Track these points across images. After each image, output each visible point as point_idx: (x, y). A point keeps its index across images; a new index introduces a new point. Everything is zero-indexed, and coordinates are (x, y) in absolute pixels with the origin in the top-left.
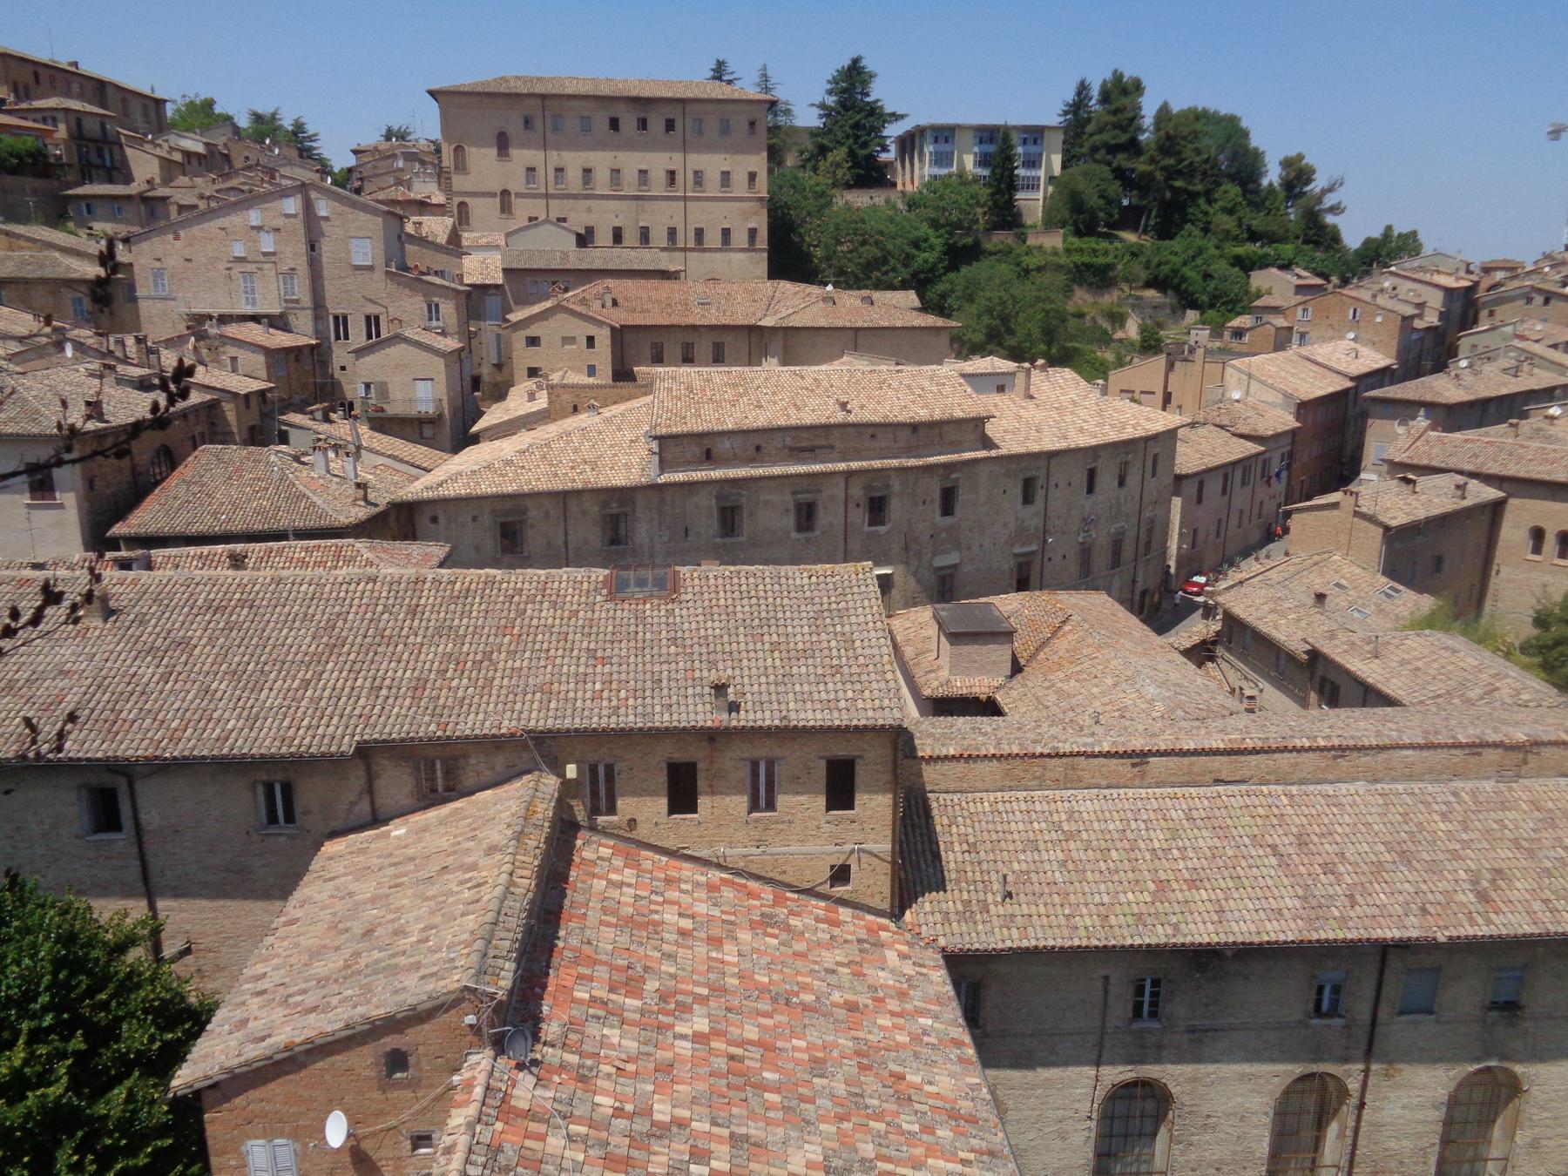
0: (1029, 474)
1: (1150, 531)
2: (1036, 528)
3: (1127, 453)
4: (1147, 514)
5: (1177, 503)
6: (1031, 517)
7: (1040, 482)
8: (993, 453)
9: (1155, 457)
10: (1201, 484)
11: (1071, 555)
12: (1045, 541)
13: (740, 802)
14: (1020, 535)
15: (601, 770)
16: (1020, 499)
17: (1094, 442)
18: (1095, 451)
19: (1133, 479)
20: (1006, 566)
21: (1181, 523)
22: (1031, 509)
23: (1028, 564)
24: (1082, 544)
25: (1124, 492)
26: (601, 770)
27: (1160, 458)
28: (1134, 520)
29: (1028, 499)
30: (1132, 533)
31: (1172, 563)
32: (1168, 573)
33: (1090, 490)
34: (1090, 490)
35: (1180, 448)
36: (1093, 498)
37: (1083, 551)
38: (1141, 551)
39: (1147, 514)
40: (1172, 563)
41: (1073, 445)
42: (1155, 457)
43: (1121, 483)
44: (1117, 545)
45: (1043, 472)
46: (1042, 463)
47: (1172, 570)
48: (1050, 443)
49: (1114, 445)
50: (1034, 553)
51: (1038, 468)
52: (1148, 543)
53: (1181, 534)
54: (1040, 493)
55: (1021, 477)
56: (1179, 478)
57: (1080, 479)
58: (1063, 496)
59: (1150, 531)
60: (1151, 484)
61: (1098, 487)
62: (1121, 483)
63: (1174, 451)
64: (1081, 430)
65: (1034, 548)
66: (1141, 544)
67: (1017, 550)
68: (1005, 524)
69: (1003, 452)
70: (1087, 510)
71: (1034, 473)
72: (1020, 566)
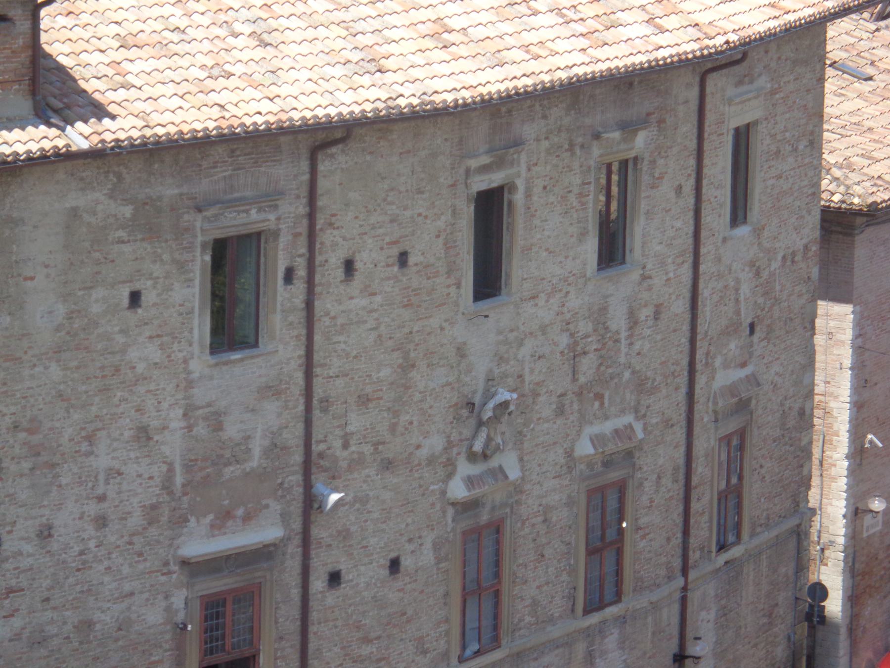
0: (233, 223)
1: (737, 445)
2: (275, 449)
3: (629, 128)
4: (721, 378)
5: (836, 325)
6: (250, 397)
7: (284, 253)
8: (80, 136)
9: (742, 139)
10: (480, 534)
11: (421, 559)
12: (311, 503)
13: (833, 468)
14: (206, 481)
15: (615, 167)
16: (201, 326)
17: (494, 82)
18: (500, 113)
19: (656, 231)
20: (154, 616)
21: (858, 406)
22: (246, 371)
23: (249, 597)
24: (469, 506)
25: (622, 287)
26: (615, 167)
27: (761, 145)
28: (668, 402)
29: (231, 327)
30: (665, 456)
31: (832, 576)
32: (815, 617)
33: (488, 282)
34: (488, 282)
35: (840, 101)
36: (499, 313)
37: (473, 535)
38: (704, 530)
39: (721, 378)
40: (832, 576)
41: (408, 98)
42: (742, 139)
43: (612, 249)
44: (606, 504)
45: (293, 208)
46: (289, 173)
47: (834, 605)
48: (313, 88)
49: (575, 93)
50: (264, 554)
51: (270, 199)
52: (731, 498)
53: (859, 454)
54: (282, 303)
55: (204, 229)
56: (840, 224)
57: (444, 234)
58: (379, 309)
59: (737, 445)
60: (732, 249)
61: (519, 270)
62: (612, 249)
63: (816, 114)
64: (440, 33)
65: (267, 531)
66: (704, 502)
67: (199, 545)
68: (143, 435)
69: (122, 128)
70: (481, 365)
71: (253, 218)
72: (214, 610)
